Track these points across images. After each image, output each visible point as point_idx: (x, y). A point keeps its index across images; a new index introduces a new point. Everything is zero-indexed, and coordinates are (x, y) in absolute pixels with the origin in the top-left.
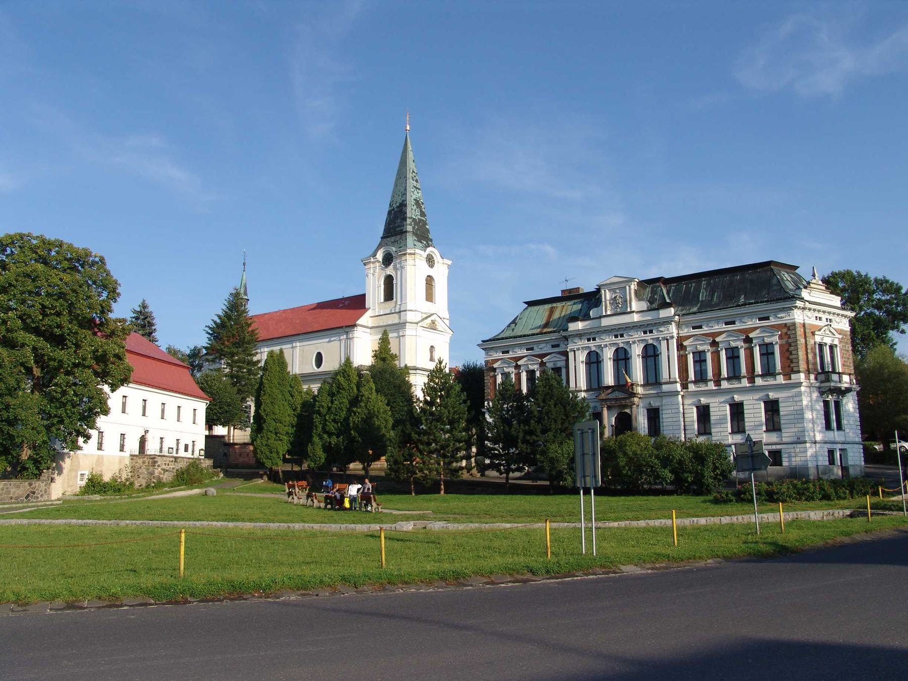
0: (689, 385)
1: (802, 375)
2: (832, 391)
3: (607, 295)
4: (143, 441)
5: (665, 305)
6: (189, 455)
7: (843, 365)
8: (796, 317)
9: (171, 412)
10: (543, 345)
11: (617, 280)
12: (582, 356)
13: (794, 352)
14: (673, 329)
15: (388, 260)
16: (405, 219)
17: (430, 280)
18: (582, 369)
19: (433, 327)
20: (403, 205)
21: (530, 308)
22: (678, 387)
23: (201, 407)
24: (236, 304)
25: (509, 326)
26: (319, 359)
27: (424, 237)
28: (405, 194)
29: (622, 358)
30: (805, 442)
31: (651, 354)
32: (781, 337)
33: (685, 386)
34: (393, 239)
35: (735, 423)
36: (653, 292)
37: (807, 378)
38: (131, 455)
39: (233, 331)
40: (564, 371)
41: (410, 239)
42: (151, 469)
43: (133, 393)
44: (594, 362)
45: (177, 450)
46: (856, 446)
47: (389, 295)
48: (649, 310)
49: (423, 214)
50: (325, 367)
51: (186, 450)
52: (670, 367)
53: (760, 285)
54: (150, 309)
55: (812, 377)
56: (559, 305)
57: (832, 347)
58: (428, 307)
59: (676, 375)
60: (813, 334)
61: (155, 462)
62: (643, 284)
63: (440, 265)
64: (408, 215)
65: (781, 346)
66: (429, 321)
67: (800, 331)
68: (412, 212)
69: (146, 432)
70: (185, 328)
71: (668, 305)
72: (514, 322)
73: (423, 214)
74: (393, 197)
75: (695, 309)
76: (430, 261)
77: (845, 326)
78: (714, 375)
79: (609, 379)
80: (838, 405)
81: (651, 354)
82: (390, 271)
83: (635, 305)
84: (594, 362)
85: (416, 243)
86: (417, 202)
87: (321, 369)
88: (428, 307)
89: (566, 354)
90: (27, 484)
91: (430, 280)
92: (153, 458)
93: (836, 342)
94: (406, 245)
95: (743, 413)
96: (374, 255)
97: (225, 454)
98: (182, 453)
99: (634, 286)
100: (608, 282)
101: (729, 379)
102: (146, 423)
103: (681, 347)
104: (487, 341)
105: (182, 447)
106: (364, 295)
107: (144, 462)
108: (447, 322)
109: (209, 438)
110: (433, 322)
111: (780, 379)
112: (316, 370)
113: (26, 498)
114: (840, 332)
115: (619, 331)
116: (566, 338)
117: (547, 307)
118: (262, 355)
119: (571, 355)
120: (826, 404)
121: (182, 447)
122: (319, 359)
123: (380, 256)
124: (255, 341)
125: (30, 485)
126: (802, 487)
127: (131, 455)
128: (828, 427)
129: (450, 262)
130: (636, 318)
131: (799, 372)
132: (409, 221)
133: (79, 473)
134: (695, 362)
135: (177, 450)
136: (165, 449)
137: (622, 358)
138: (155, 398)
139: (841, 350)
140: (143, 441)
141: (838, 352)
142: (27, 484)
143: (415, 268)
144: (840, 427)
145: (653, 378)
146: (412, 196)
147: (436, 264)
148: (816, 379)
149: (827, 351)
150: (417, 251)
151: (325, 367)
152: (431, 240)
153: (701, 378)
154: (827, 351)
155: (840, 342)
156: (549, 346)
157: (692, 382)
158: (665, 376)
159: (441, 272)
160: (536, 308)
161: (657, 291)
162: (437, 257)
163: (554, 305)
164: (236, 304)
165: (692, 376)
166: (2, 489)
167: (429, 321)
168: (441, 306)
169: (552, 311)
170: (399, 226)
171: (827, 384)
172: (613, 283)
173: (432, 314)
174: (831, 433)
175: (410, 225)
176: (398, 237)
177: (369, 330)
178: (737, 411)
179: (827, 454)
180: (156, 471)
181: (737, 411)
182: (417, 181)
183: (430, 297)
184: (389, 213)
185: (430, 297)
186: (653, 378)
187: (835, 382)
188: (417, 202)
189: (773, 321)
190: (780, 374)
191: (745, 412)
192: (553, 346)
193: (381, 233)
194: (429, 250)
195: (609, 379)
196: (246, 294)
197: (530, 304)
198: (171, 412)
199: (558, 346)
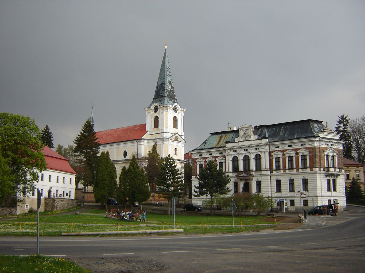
0: (273, 171)
1: (317, 169)
2: (332, 175)
3: (241, 133)
4: (50, 192)
5: (265, 138)
6: (68, 197)
7: (338, 164)
8: (316, 144)
9: (61, 179)
10: (216, 153)
11: (245, 126)
12: (231, 158)
13: (314, 159)
14: (267, 148)
15: (156, 109)
16: (164, 90)
17: (175, 119)
18: (231, 164)
19: (176, 139)
20: (163, 84)
21: (212, 136)
22: (269, 172)
23: (73, 177)
24: (89, 127)
25: (203, 144)
26: (125, 154)
27: (173, 98)
28: (164, 78)
29: (247, 159)
30: (317, 196)
31: (258, 158)
32: (310, 152)
33: (271, 172)
34: (158, 99)
35: (291, 186)
36: (262, 131)
37: (320, 170)
38: (45, 198)
39: (88, 140)
40: (224, 164)
41: (166, 100)
42: (53, 203)
43: (46, 173)
44: (235, 160)
45: (63, 195)
46: (343, 198)
47: (156, 125)
48: (258, 139)
49: (172, 87)
50: (128, 157)
51: (67, 195)
52: (265, 163)
53: (303, 128)
54: (50, 130)
55: (322, 169)
56: (224, 135)
57: (333, 156)
58: (175, 131)
59: (268, 167)
60: (324, 152)
61: (55, 201)
62: (257, 128)
63: (180, 111)
64: (166, 88)
65: (310, 156)
66: (174, 137)
67: (317, 150)
68: (168, 87)
69: (51, 188)
70: (66, 136)
71: (266, 138)
72: (205, 142)
73: (172, 87)
74: (159, 79)
75: (277, 140)
76: (175, 110)
77: (341, 147)
78: (283, 168)
79: (241, 168)
80: (334, 181)
81: (258, 158)
82: (156, 114)
83: (253, 137)
84: (235, 160)
85: (169, 101)
86: (170, 82)
87: (126, 158)
88: (175, 131)
89: (224, 157)
90: (9, 209)
91: (175, 119)
92: (54, 199)
93: (335, 154)
94: (164, 103)
95: (281, 184)
96: (150, 107)
97: (83, 197)
98: (65, 197)
99: (252, 129)
100: (242, 127)
101: (289, 169)
102: (50, 184)
103: (270, 155)
104: (193, 150)
105: (65, 194)
106: (145, 125)
107: (50, 201)
108: (183, 137)
109: (77, 189)
110: (176, 137)
111: (308, 170)
112: (124, 158)
113: (9, 214)
114: (338, 150)
115: (246, 148)
116: (225, 150)
117: (219, 136)
118: (102, 149)
119: (227, 157)
120: (329, 181)
121: (65, 194)
122: (125, 154)
123: (152, 107)
124: (98, 145)
125: (10, 209)
126: (230, 210)
127: (45, 198)
128: (329, 190)
129: (184, 110)
130: (252, 142)
131: (316, 167)
132: (166, 91)
133: (26, 205)
134: (276, 162)
135: (63, 195)
136: (58, 195)
137: (247, 159)
138: (54, 174)
139: (337, 157)
140: (50, 192)
141: (336, 159)
142: (9, 209)
143: (168, 115)
144: (335, 190)
145: (259, 168)
146: (168, 79)
147: (178, 111)
148: (324, 170)
149: (330, 158)
150: (169, 106)
151: (128, 157)
152: (176, 99)
153: (278, 168)
154: (330, 158)
155: (337, 154)
156: (218, 153)
157: (274, 170)
158: (263, 167)
159: (180, 115)
160: (215, 136)
161: (260, 130)
162: (179, 108)
163: (222, 135)
164: (89, 127)
165: (274, 167)
166: (1, 211)
167: (174, 137)
168: (180, 130)
169: (221, 137)
170: (161, 94)
171: (328, 172)
172: (244, 128)
173: (176, 134)
174: (330, 192)
175: (167, 93)
176: (161, 99)
177: (147, 141)
178: (292, 183)
179: (327, 201)
180: (55, 205)
181: (292, 183)
182: (170, 72)
183: (175, 126)
184: (157, 87)
185: (175, 126)
186: (259, 168)
187: (332, 171)
188: (170, 82)
189: (307, 146)
190: (295, 169)
191: (282, 184)
192: (220, 153)
193: (153, 96)
194: (175, 105)
195: (241, 168)
196: (93, 122)
197: (213, 134)
198: (61, 179)
199: (222, 153)
